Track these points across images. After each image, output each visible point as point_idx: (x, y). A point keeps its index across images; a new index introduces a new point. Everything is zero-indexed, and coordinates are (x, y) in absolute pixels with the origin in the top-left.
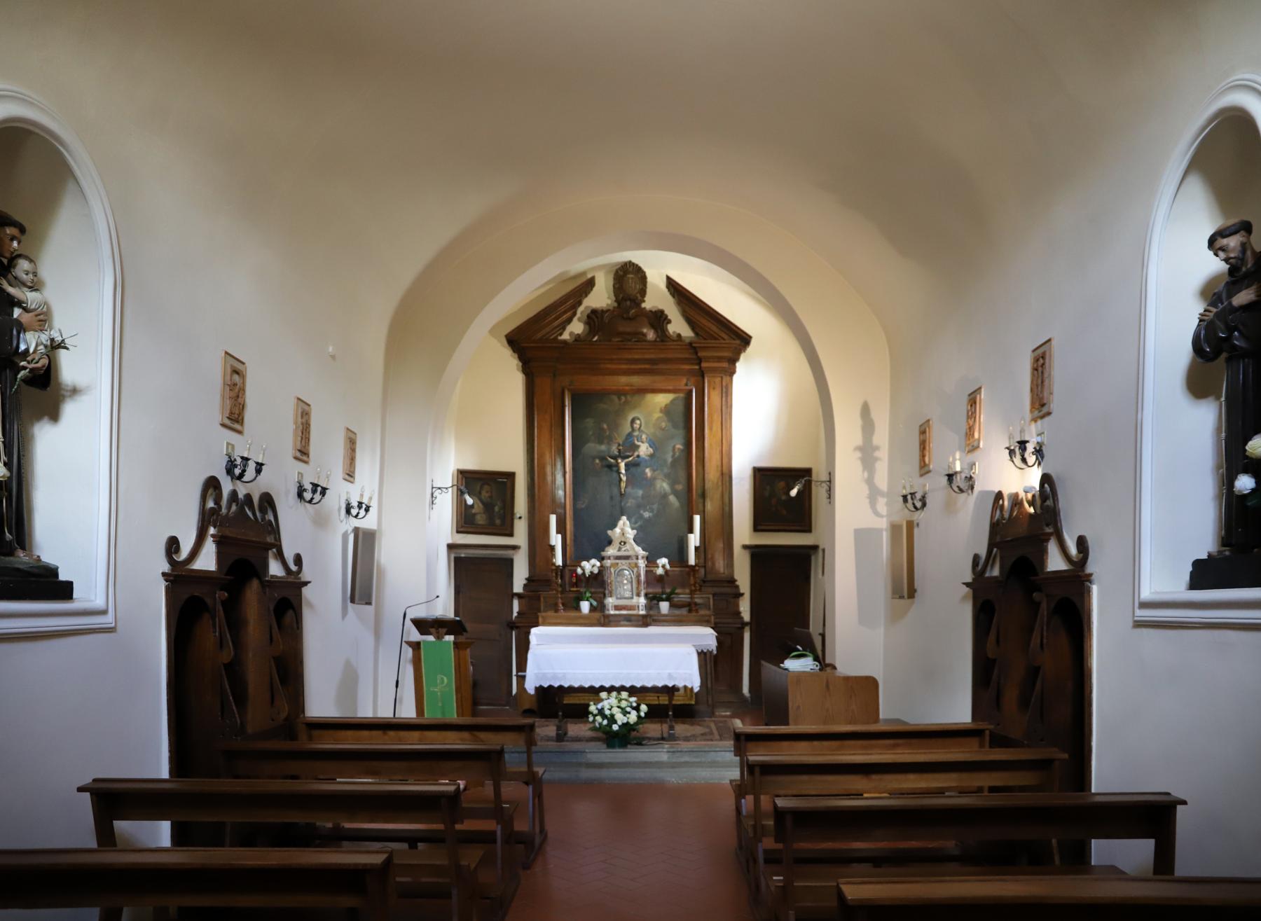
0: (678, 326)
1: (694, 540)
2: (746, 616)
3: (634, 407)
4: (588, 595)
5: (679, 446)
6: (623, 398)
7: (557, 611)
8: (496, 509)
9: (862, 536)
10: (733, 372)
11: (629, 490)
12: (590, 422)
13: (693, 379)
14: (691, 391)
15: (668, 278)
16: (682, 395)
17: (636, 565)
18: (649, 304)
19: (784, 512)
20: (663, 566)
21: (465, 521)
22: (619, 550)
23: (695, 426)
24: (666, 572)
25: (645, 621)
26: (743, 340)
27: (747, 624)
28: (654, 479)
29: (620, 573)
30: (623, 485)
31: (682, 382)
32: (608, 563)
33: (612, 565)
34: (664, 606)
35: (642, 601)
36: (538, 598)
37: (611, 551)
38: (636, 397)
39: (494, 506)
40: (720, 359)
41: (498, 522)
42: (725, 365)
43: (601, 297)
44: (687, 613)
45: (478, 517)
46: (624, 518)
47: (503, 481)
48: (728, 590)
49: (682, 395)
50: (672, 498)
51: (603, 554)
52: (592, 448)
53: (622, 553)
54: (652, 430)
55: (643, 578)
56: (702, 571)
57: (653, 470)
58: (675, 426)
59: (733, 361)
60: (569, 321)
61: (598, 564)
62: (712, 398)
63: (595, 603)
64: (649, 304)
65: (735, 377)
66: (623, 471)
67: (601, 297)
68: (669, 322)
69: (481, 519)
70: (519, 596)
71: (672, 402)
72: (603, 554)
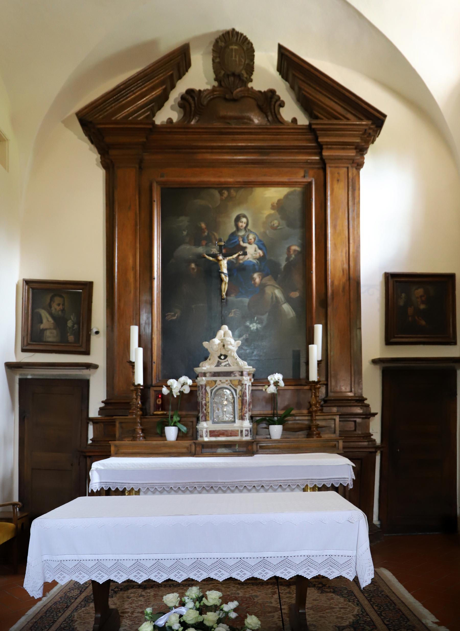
0: (291, 111)
1: (316, 352)
2: (377, 437)
3: (240, 203)
4: (176, 419)
5: (295, 248)
6: (226, 193)
7: (134, 438)
8: (70, 324)
10: (360, 165)
11: (232, 298)
12: (184, 221)
13: (311, 172)
14: (310, 184)
15: (281, 49)
16: (298, 189)
17: (240, 383)
18: (259, 84)
19: (423, 323)
20: (276, 384)
21: (32, 338)
22: (219, 364)
23: (313, 220)
24: (279, 390)
25: (249, 449)
26: (376, 119)
27: (377, 448)
28: (262, 286)
29: (218, 392)
30: (225, 287)
31: (299, 177)
32: (202, 381)
33: (208, 383)
34: (276, 431)
35: (247, 424)
36: (112, 424)
37: (206, 367)
38: (242, 192)
39: (66, 321)
40: (344, 145)
41: (71, 338)
42: (352, 153)
43: (200, 76)
44: (305, 437)
45: (48, 333)
46: (225, 327)
47: (80, 292)
48: (359, 410)
49: (298, 189)
50: (286, 307)
51: (198, 370)
52: (187, 250)
53: (221, 369)
54: (262, 230)
55: (248, 398)
56: (323, 390)
57: (263, 277)
58: (290, 224)
59: (362, 150)
60: (160, 106)
61: (190, 382)
62: (336, 192)
63: (184, 429)
64: (259, 84)
65: (362, 171)
66: (225, 270)
67: (200, 76)
68: (282, 104)
69: (51, 336)
70: (95, 421)
71: (286, 197)
72: (198, 370)
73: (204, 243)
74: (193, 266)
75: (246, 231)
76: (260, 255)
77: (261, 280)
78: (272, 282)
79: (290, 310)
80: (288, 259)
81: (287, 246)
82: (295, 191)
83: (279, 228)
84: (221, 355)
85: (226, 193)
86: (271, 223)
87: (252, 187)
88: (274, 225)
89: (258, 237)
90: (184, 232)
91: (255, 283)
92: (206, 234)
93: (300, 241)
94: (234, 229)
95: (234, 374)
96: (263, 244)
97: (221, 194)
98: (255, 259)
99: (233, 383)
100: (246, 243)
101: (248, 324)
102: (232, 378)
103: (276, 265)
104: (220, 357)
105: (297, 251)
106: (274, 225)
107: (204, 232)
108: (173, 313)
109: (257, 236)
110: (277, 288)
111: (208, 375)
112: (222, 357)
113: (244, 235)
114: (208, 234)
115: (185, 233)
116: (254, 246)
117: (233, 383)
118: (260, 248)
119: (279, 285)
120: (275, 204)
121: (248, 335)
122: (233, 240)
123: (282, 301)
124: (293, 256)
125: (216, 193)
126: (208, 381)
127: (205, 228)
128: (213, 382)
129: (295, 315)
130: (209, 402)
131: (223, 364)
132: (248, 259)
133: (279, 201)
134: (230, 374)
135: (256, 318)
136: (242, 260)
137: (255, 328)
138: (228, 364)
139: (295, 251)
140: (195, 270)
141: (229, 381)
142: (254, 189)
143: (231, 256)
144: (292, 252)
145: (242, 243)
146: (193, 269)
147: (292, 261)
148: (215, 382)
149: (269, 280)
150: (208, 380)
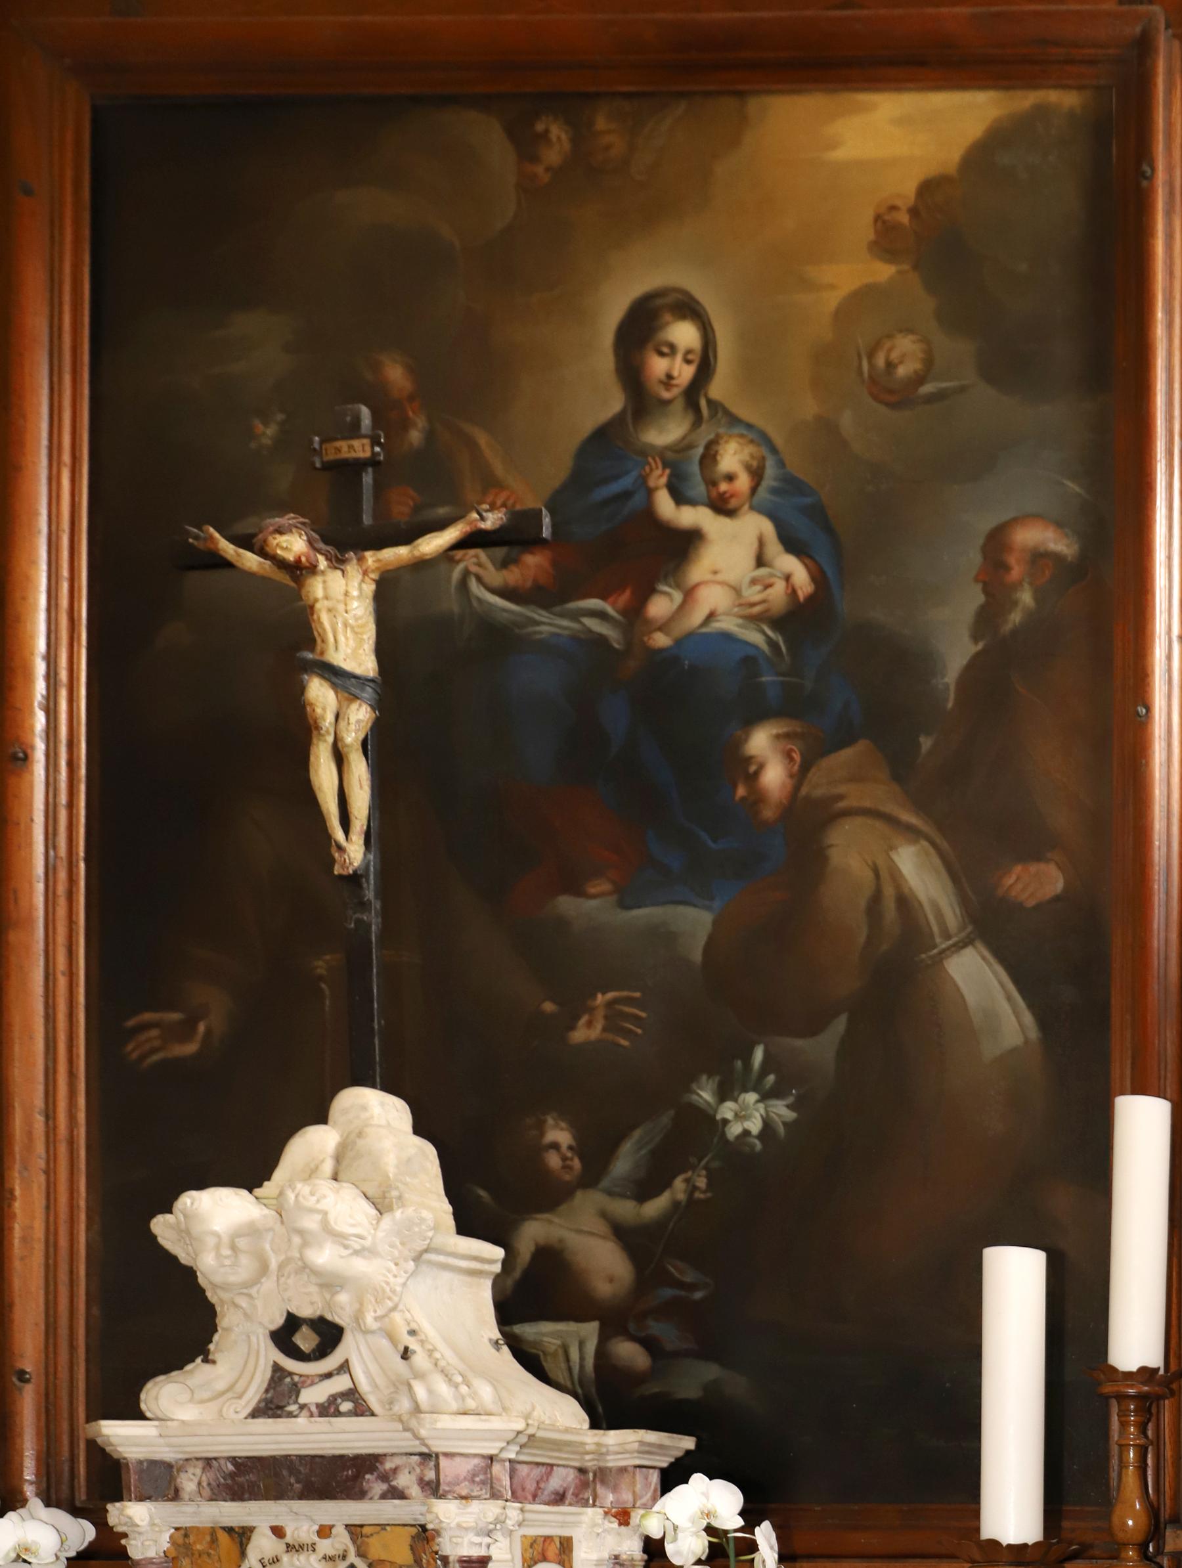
9: (738, 626)
12: (260, 345)
16: (1065, 100)
22: (275, 1402)
28: (807, 820)
50: (975, 978)
53: (300, 1435)
54: (809, 408)
57: (807, 757)
71: (983, 157)
75: (698, 421)
76: (794, 592)
77: (800, 776)
78: (880, 793)
79: (1005, 1008)
80: (986, 620)
81: (986, 523)
82: (1041, 111)
83: (927, 388)
84: (292, 1323)
86: (871, 355)
87: (741, 95)
88: (890, 366)
89: (781, 464)
90: (259, 427)
91: (757, 798)
93: (1073, 487)
94: (615, 403)
95: (385, 1478)
96: (817, 514)
97: (527, 145)
98: (754, 620)
100: (692, 503)
101: (705, 1095)
102: (371, 1510)
103: (907, 661)
105: (1057, 557)
106: (890, 366)
108: (175, 1016)
109: (774, 450)
110: (912, 833)
111: (188, 1483)
112: (305, 1340)
113: (682, 448)
114: (430, 435)
115: (267, 432)
116: (754, 526)
117: (376, 1550)
118: (791, 544)
119: (920, 805)
120: (904, 218)
121: (702, 1182)
122: (606, 481)
123: (947, 936)
124: (1026, 597)
125: (488, 137)
127: (411, 398)
128: (223, 1538)
129: (1034, 1034)
131: (313, 1395)
132: (711, 616)
133: (927, 188)
134: (358, 1477)
135: (758, 1055)
136: (663, 628)
137: (755, 1126)
138: (352, 1394)
139: (1038, 557)
142: (754, 104)
144: (1017, 571)
145: (665, 505)
147: (1015, 632)
148: (242, 1536)
149: (847, 772)
150: (186, 1521)
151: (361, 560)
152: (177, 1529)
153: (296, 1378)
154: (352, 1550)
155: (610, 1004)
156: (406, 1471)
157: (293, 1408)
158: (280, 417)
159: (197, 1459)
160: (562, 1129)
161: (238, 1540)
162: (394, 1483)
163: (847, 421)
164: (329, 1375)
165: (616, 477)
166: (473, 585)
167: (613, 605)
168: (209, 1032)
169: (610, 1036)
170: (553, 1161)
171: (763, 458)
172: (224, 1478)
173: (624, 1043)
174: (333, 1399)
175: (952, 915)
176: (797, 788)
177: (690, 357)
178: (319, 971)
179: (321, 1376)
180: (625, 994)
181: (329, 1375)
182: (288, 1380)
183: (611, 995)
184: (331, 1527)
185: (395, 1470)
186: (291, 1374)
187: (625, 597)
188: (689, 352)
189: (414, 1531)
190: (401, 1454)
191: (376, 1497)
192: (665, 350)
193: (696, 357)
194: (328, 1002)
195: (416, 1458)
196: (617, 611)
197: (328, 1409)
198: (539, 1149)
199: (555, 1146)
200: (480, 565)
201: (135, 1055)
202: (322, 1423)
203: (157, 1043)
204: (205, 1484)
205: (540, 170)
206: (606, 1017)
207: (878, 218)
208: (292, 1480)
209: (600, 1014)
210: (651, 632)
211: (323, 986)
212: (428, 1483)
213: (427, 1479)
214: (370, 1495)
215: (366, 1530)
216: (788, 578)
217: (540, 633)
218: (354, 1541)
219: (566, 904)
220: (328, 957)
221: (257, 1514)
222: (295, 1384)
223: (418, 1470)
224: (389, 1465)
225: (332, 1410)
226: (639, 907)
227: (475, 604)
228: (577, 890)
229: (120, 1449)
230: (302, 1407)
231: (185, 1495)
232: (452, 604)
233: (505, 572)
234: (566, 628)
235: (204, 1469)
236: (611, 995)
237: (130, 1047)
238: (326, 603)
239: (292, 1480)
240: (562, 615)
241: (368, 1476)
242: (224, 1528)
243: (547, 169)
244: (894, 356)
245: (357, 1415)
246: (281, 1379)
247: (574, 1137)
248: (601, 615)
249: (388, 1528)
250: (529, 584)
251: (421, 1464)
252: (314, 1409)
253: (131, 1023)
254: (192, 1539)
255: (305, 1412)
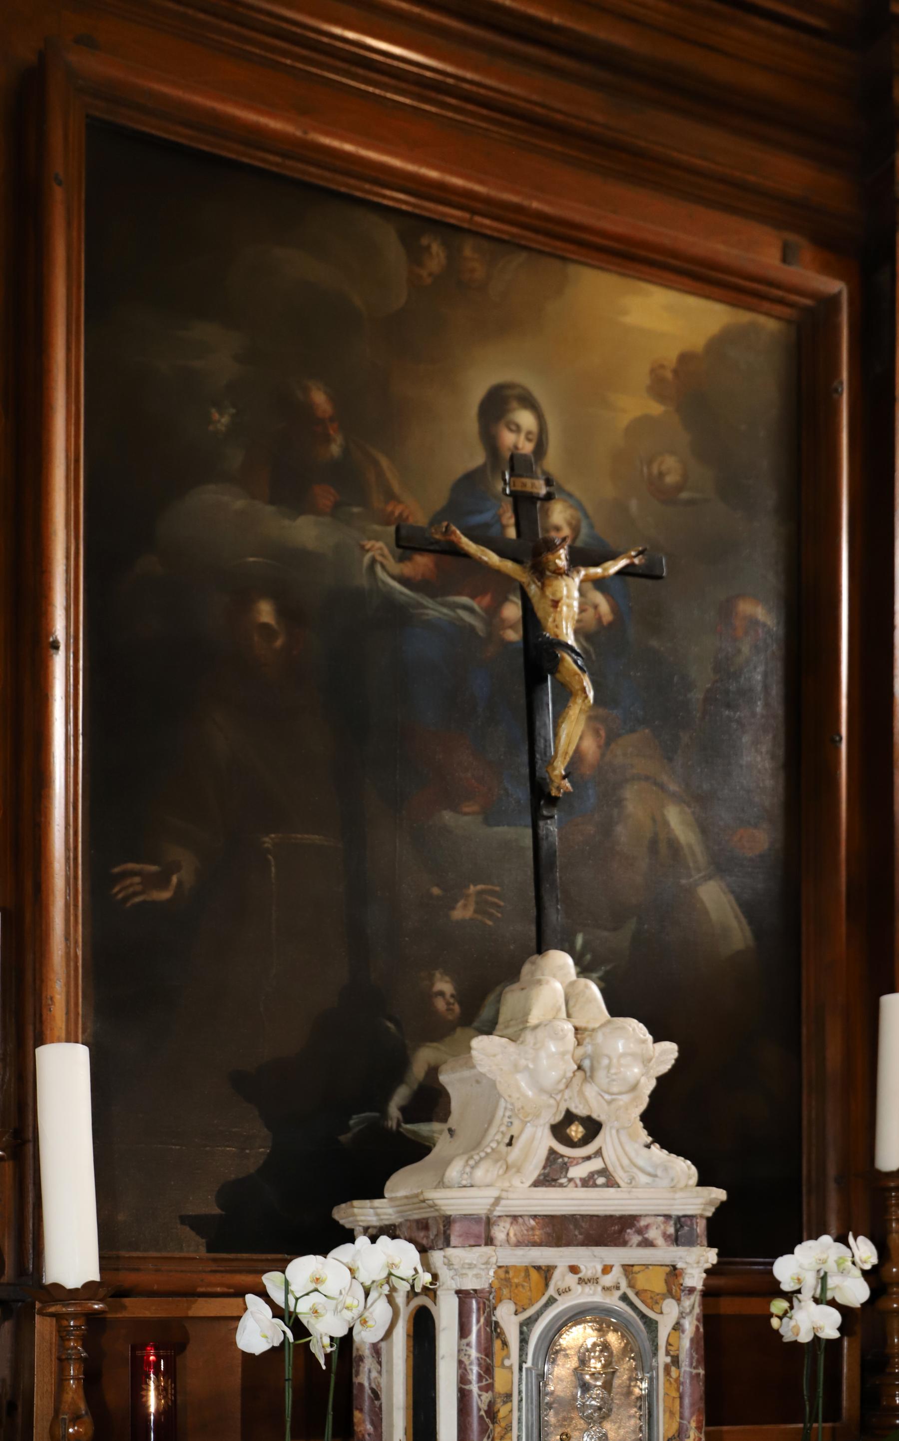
6: (437, 254)
12: (216, 352)
22: (552, 1173)
52: (226, 514)
71: (720, 344)
73: (325, 496)
74: (266, 612)
76: (599, 619)
79: (734, 924)
84: (570, 1117)
85: (437, 254)
86: (650, 463)
88: (661, 475)
89: (591, 526)
92: (335, 449)
94: (478, 458)
95: (640, 1232)
97: (416, 255)
99: (642, 1281)
102: (632, 1254)
104: (559, 1131)
107: (328, 440)
108: (154, 868)
109: (586, 516)
110: (676, 798)
111: (499, 1233)
114: (346, 450)
115: (222, 420)
117: (642, 1281)
120: (669, 375)
125: (388, 238)
126: (506, 1269)
128: (534, 1275)
129: (751, 942)
130: (508, 1397)
131: (578, 1172)
133: (685, 358)
134: (622, 1231)
140: (279, 643)
141: (616, 1276)
143: (596, 565)
146: (640, 560)
148: (546, 1273)
149: (634, 753)
151: (578, 572)
152: (500, 1267)
153: (566, 1159)
154: (624, 1284)
155: (480, 893)
156: (654, 1227)
157: (563, 1181)
158: (233, 411)
159: (507, 1216)
160: (447, 982)
161: (544, 1275)
162: (646, 1236)
163: (634, 505)
164: (588, 1158)
165: (481, 512)
166: (379, 569)
167: (479, 604)
168: (180, 883)
169: (479, 917)
170: (440, 1004)
171: (579, 521)
172: (527, 1230)
173: (490, 923)
174: (592, 1175)
175: (701, 857)
176: (603, 755)
177: (530, 437)
178: (266, 845)
179: (583, 1158)
180: (490, 887)
181: (588, 1158)
182: (560, 1160)
183: (480, 887)
184: (612, 1267)
185: (647, 1227)
186: (562, 1156)
187: (487, 600)
188: (529, 433)
189: (668, 1269)
190: (652, 1215)
191: (635, 1245)
192: (513, 427)
193: (534, 437)
194: (273, 869)
195: (661, 1218)
196: (482, 608)
197: (588, 1182)
198: (429, 996)
199: (441, 994)
200: (383, 555)
201: (120, 896)
202: (583, 1193)
203: (138, 888)
204: (512, 1234)
205: (424, 273)
206: (477, 903)
207: (653, 371)
208: (577, 1233)
209: (472, 900)
210: (504, 628)
211: (270, 857)
212: (669, 1236)
213: (668, 1233)
214: (630, 1244)
215: (636, 1269)
216: (596, 607)
217: (427, 615)
218: (627, 1276)
219: (447, 816)
220: (273, 836)
221: (558, 1257)
222: (565, 1164)
223: (662, 1227)
224: (643, 1223)
225: (591, 1183)
226: (499, 826)
227: (380, 584)
228: (455, 808)
229: (443, 1208)
230: (570, 1180)
231: (497, 1242)
232: (363, 581)
233: (401, 565)
234: (445, 615)
235: (512, 1223)
236: (480, 887)
237: (116, 889)
238: (567, 601)
239: (577, 1233)
240: (443, 605)
241: (629, 1231)
242: (534, 1267)
243: (430, 274)
244: (664, 468)
245: (608, 1186)
246: (555, 1160)
247: (456, 989)
248: (470, 610)
249: (651, 1267)
250: (419, 577)
251: (665, 1223)
252: (578, 1182)
253: (116, 870)
254: (511, 1274)
255: (572, 1184)
